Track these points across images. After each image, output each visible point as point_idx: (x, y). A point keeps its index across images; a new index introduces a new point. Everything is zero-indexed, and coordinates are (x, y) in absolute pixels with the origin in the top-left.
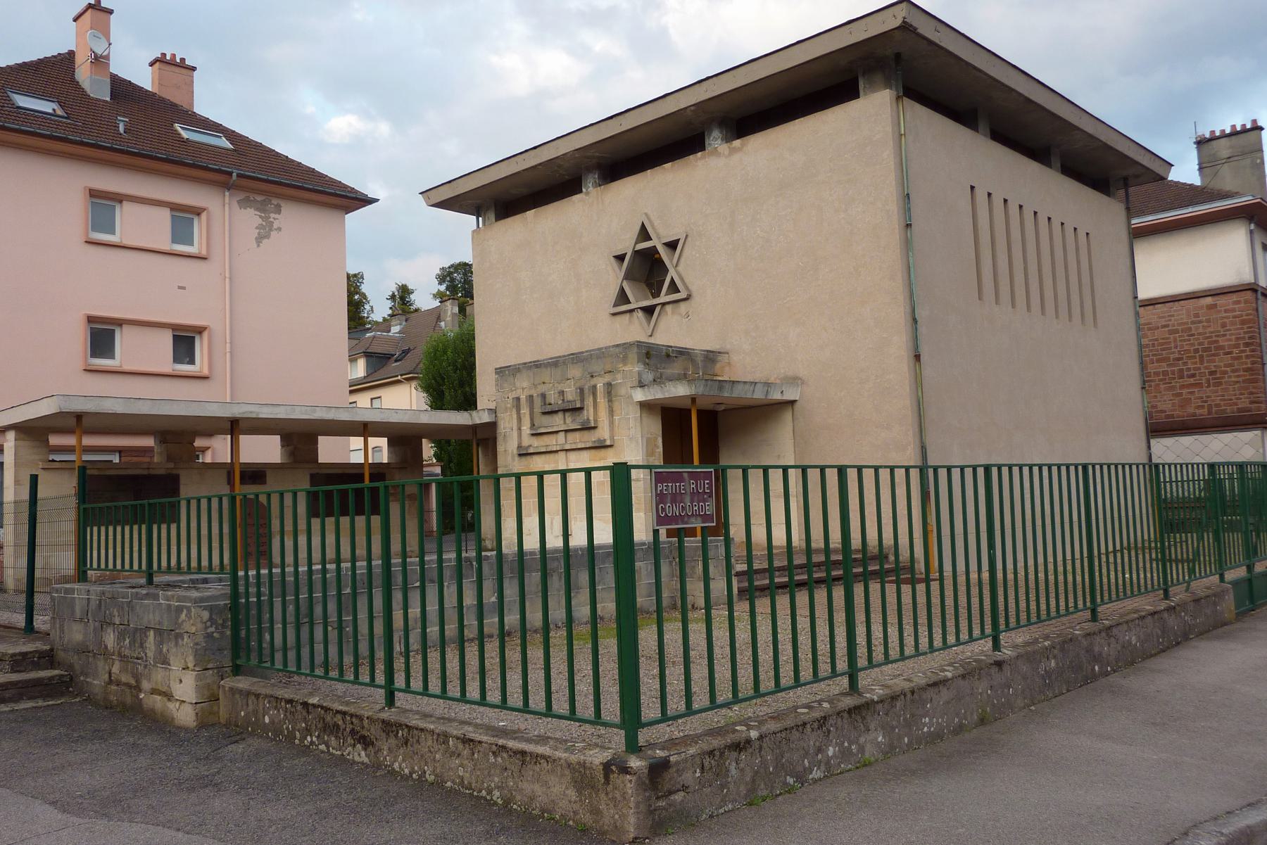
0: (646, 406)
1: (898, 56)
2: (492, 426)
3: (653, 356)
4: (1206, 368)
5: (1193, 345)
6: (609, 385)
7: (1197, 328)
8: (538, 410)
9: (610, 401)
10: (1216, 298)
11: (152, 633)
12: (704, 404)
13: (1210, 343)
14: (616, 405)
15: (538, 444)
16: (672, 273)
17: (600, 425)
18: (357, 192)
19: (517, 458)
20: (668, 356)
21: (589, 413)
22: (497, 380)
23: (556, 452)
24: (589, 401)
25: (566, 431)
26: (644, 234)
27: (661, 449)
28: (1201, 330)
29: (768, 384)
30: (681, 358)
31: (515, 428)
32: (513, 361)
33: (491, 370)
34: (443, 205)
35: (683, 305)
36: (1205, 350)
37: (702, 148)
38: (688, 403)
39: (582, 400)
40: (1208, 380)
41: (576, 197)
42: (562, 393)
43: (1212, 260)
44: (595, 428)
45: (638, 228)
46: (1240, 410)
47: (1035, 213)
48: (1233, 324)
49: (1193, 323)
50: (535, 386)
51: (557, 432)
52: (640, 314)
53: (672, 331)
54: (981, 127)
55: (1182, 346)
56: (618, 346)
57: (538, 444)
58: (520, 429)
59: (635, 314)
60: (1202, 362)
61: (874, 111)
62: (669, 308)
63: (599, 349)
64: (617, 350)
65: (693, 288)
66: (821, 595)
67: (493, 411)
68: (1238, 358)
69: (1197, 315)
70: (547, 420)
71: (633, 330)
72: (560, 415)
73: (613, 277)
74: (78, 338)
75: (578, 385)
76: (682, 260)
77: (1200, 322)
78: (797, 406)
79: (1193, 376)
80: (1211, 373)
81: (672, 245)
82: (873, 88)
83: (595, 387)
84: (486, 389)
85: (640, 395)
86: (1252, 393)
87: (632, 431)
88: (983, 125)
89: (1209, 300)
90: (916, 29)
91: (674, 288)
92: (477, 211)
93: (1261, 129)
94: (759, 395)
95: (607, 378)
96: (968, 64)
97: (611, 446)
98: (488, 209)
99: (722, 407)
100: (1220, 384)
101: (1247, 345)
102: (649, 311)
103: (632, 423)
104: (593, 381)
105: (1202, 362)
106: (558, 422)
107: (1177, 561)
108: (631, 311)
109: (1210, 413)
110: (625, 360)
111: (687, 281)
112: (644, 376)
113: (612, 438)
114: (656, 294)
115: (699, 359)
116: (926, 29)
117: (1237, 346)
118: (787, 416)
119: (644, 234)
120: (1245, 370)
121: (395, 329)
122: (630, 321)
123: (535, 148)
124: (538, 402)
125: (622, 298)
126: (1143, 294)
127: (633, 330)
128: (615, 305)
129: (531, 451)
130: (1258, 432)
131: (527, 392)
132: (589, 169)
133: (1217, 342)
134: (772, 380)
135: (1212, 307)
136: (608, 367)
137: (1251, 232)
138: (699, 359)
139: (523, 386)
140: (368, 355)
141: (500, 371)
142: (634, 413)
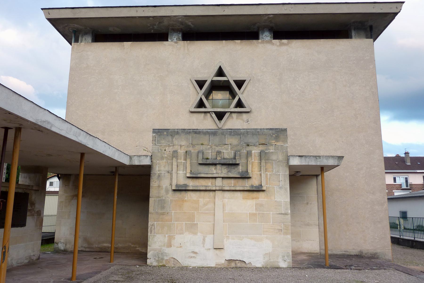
15: (192, 184)
19: (171, 193)
23: (215, 191)
25: (223, 178)
35: (245, 116)
37: (167, 40)
41: (255, 41)
44: (250, 178)
45: (217, 68)
50: (193, 146)
52: (214, 115)
57: (192, 184)
62: (234, 115)
63: (174, 129)
64: (271, 132)
87: (282, 183)
104: (249, 148)
108: (205, 112)
122: (204, 117)
132: (175, 30)
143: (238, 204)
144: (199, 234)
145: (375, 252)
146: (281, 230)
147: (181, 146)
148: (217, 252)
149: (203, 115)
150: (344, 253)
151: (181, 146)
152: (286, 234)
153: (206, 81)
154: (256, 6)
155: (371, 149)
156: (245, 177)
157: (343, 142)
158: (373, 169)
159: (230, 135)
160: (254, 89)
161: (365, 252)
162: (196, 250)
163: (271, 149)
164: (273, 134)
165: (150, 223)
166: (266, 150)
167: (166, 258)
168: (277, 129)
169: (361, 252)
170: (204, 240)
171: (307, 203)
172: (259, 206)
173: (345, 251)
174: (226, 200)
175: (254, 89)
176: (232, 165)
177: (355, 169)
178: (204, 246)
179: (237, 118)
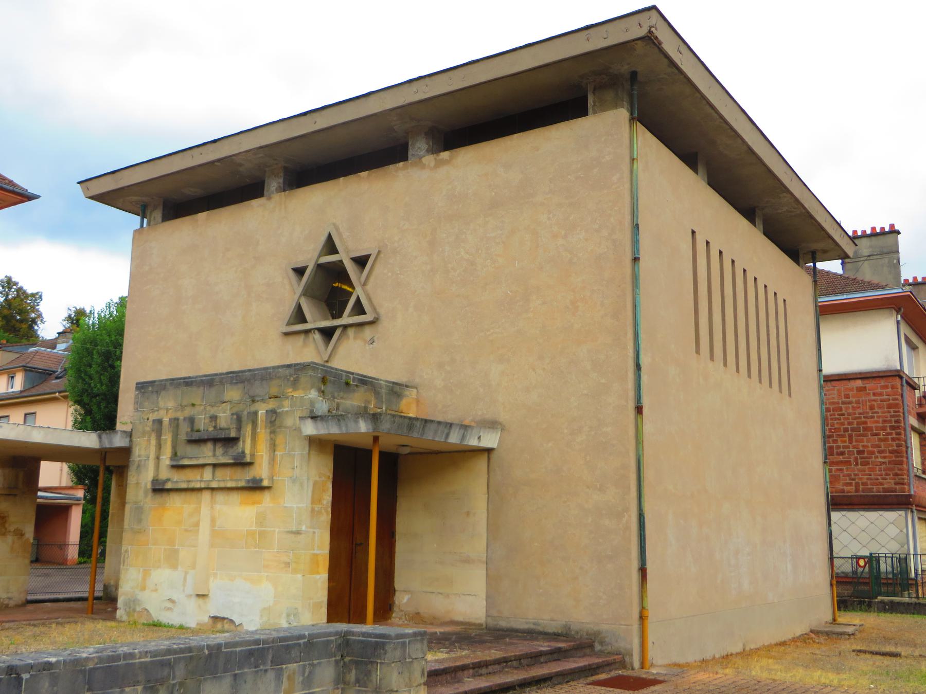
0: (316, 443)
1: (634, 75)
2: (126, 452)
3: (332, 380)
4: (854, 447)
5: (843, 424)
6: (273, 413)
7: (847, 408)
8: (183, 437)
9: (273, 432)
10: (865, 382)
12: (389, 442)
13: (858, 423)
14: (279, 440)
15: (179, 479)
16: (359, 291)
17: (257, 462)
18: (14, 185)
19: (150, 494)
20: (347, 384)
21: (246, 445)
22: (136, 397)
23: (200, 490)
24: (248, 430)
25: (215, 466)
26: (330, 246)
27: (330, 499)
28: (851, 411)
29: (465, 428)
30: (362, 389)
31: (152, 455)
32: (162, 374)
33: (133, 386)
34: (102, 198)
35: (368, 332)
36: (853, 430)
38: (367, 443)
39: (239, 429)
40: (856, 459)
41: (255, 203)
42: (214, 418)
43: (866, 345)
45: (323, 238)
46: (885, 490)
48: (880, 407)
49: (843, 403)
51: (203, 466)
52: (317, 336)
53: (352, 355)
54: (701, 169)
55: (833, 425)
56: (289, 366)
57: (179, 479)
58: (158, 458)
59: (311, 335)
60: (851, 442)
61: (607, 132)
62: (351, 332)
63: (266, 369)
64: (288, 371)
65: (382, 311)
67: (130, 435)
68: (886, 440)
69: (847, 396)
70: (191, 450)
71: (308, 351)
72: (210, 446)
73: (289, 293)
75: (235, 410)
76: (372, 279)
77: (850, 403)
78: (494, 455)
79: (842, 453)
80: (859, 452)
81: (361, 262)
82: (603, 107)
83: (256, 413)
84: (127, 410)
85: (310, 429)
86: (897, 475)
88: (701, 169)
89: (859, 383)
90: (660, 43)
91: (359, 309)
92: (142, 211)
93: (899, 233)
94: (454, 438)
95: (272, 404)
96: (703, 97)
97: (268, 488)
98: (155, 208)
99: (407, 451)
100: (868, 463)
101: (892, 428)
102: (327, 333)
103: (297, 463)
105: (851, 442)
106: (207, 454)
108: (307, 332)
109: (857, 491)
110: (295, 384)
111: (375, 302)
112: (318, 406)
113: (271, 478)
114: (338, 315)
115: (384, 391)
116: (670, 47)
117: (884, 429)
118: (481, 464)
119: (330, 246)
120: (890, 452)
121: (61, 347)
123: (215, 141)
124: (184, 428)
125: (299, 316)
126: (829, 368)
127: (308, 351)
128: (289, 324)
129: (169, 486)
130: (902, 513)
131: (172, 415)
133: (865, 423)
134: (466, 422)
135: (860, 389)
136: (274, 391)
137: (898, 322)
138: (384, 391)
139: (167, 407)
140: (27, 369)
141: (142, 387)
142: (300, 449)
143: (238, 513)
144: (180, 568)
145: (596, 628)
146: (289, 563)
147: (167, 410)
148: (201, 601)
149: (302, 337)
150: (532, 626)
151: (167, 410)
152: (295, 571)
153: (307, 267)
154: (364, 99)
155: (603, 381)
156: (241, 463)
157: (544, 369)
158: (604, 429)
159: (231, 383)
160: (385, 271)
161: (575, 627)
162: (174, 598)
163: (286, 406)
164: (291, 375)
165: (124, 548)
166: (279, 407)
167: (138, 609)
168: (297, 364)
169: (567, 627)
170: (185, 579)
171: (468, 514)
172: (261, 519)
173: (534, 624)
174: (218, 507)
175: (385, 271)
176: (229, 441)
177: (566, 431)
178: (184, 591)
179: (355, 338)
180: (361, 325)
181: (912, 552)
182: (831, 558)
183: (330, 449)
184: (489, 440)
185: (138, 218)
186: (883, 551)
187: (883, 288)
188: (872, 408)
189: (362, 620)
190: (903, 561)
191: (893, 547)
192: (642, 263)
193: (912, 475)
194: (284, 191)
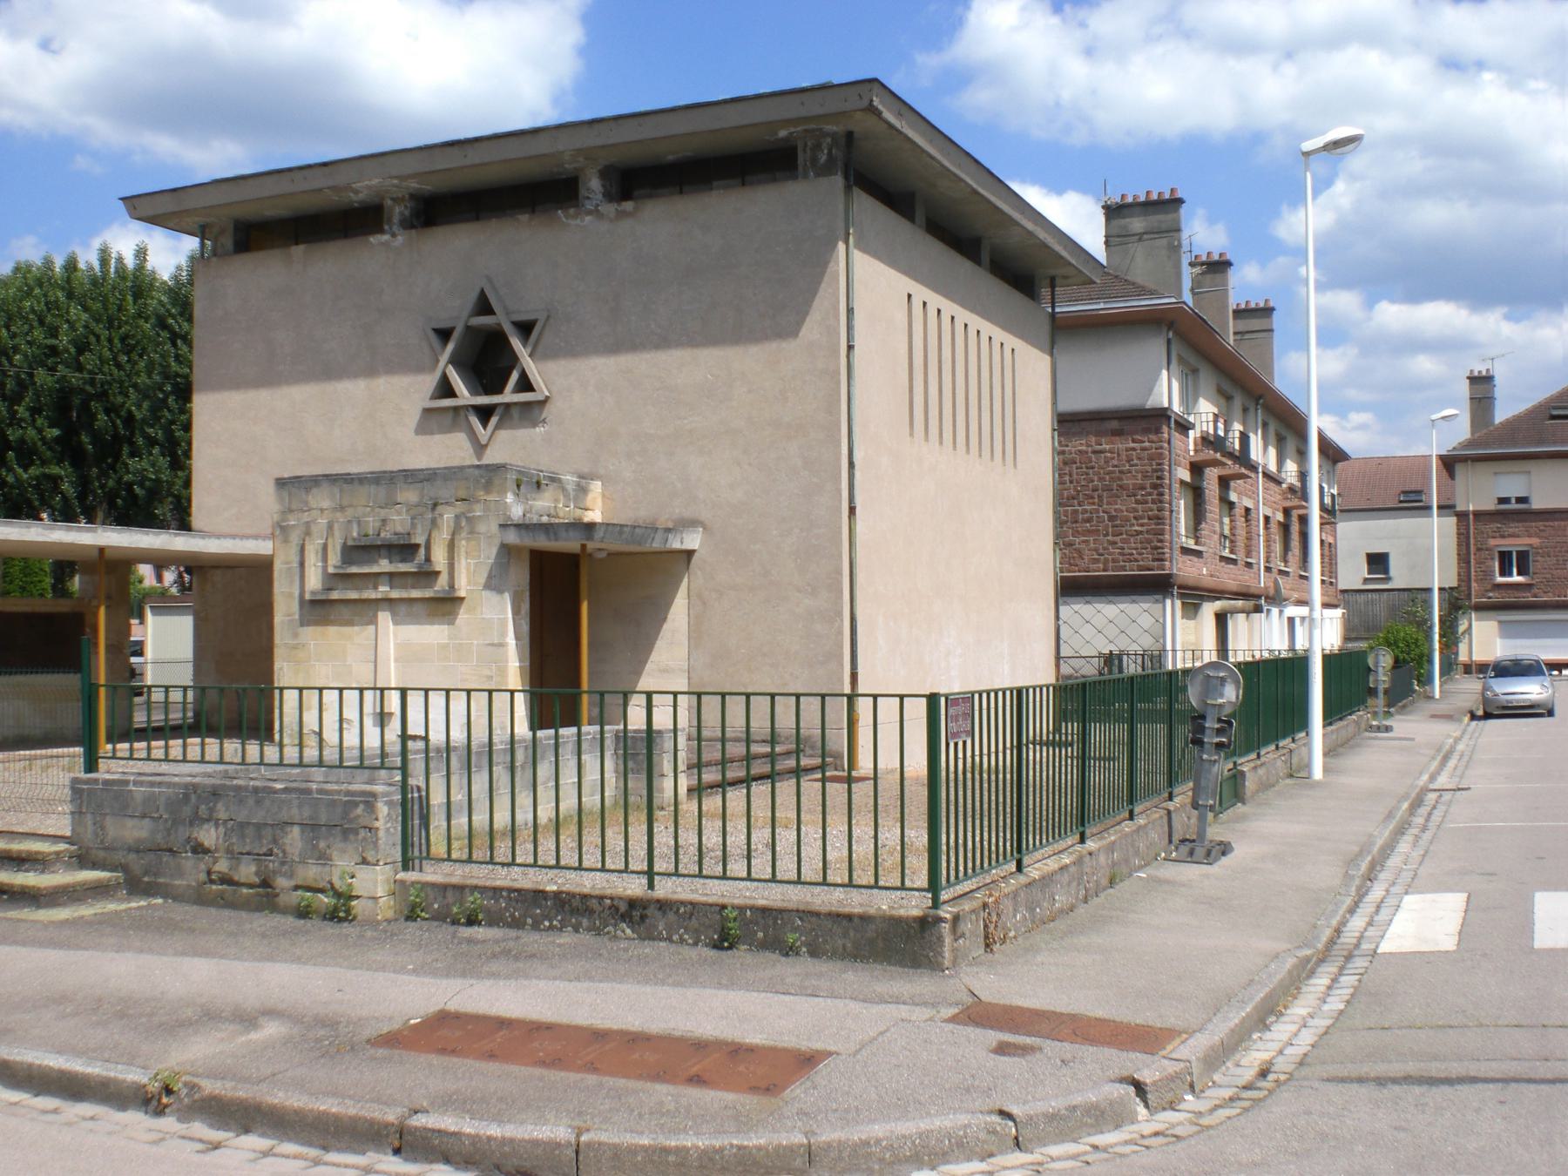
11: (296, 830)
26: (484, 307)
46: (1141, 568)
47: (909, 296)
49: (1094, 452)
52: (451, 414)
64: (477, 472)
66: (786, 788)
74: (1557, 711)
80: (1112, 518)
86: (1157, 548)
91: (525, 385)
94: (656, 545)
102: (485, 413)
107: (1047, 744)
119: (484, 307)
128: (435, 397)
136: (462, 494)
137: (1169, 342)
151: (322, 510)
180: (527, 405)
181: (1169, 647)
182: (1058, 657)
183: (526, 556)
184: (692, 540)
185: (197, 240)
186: (1134, 647)
187: (1152, 293)
188: (1129, 460)
189: (1510, 575)
190: (1158, 657)
191: (1147, 642)
192: (857, 350)
193: (1176, 547)
194: (412, 227)
